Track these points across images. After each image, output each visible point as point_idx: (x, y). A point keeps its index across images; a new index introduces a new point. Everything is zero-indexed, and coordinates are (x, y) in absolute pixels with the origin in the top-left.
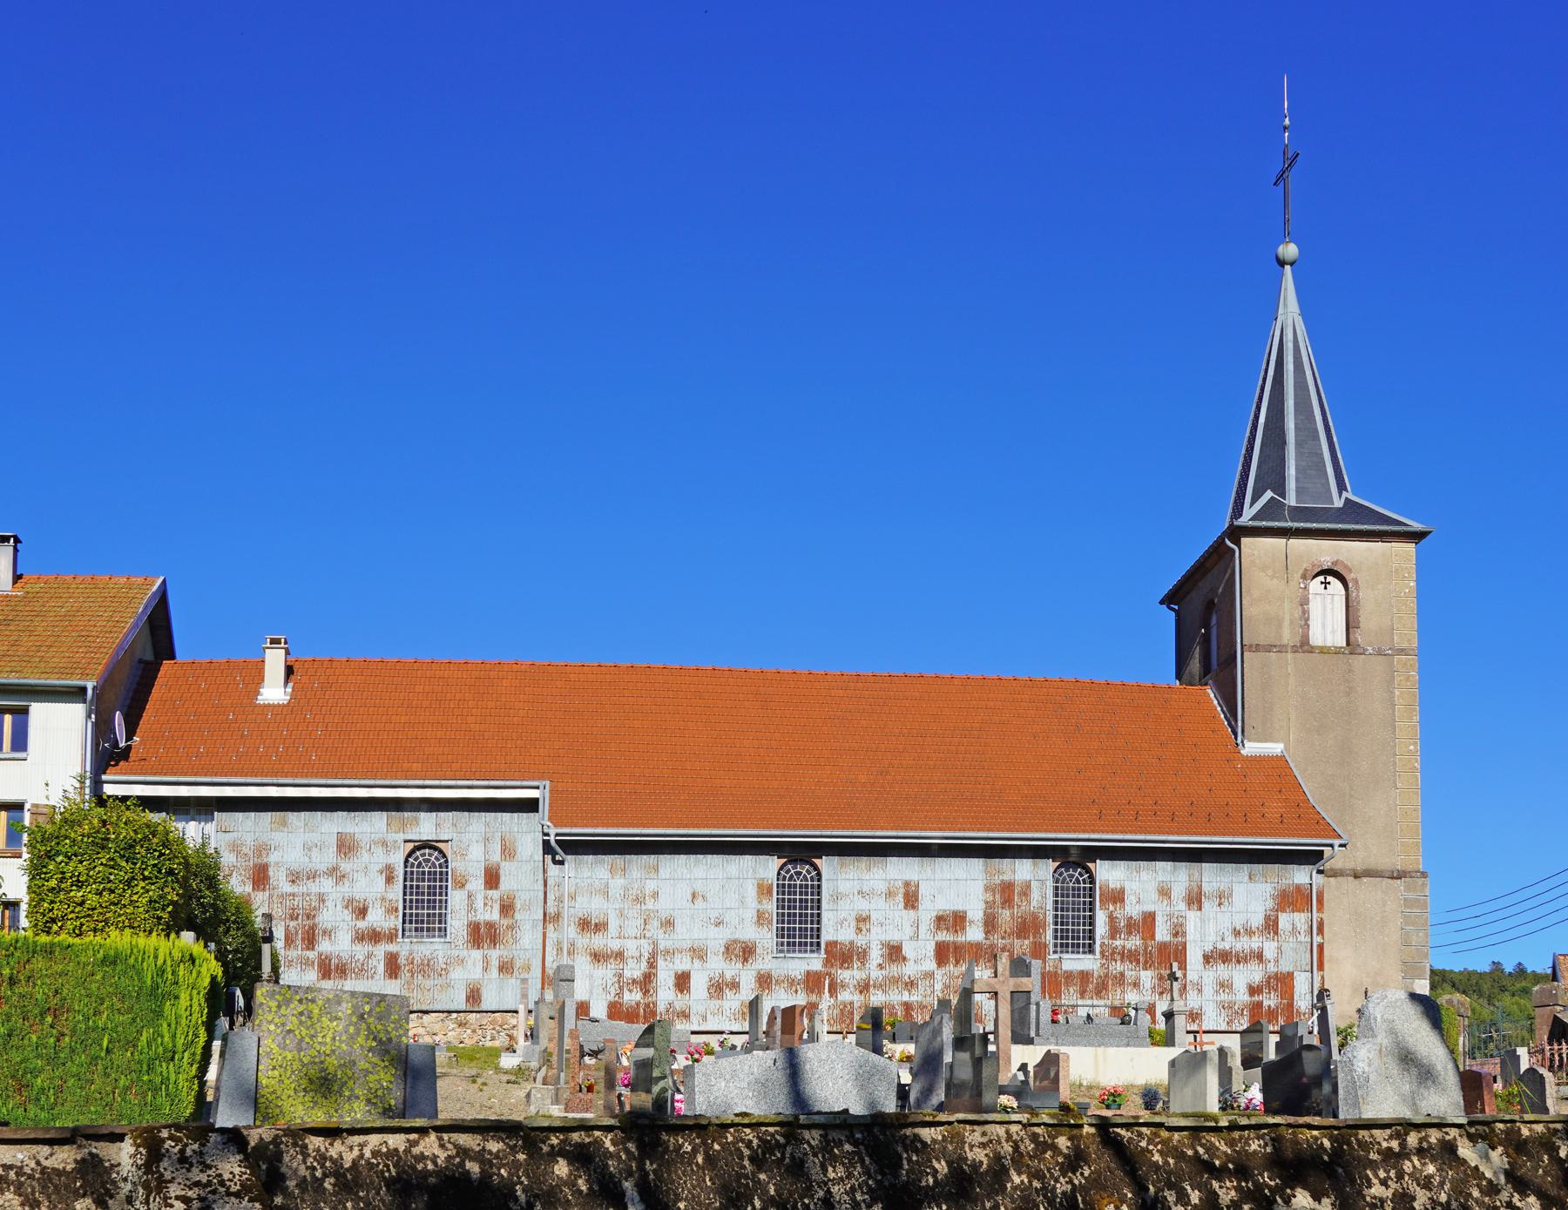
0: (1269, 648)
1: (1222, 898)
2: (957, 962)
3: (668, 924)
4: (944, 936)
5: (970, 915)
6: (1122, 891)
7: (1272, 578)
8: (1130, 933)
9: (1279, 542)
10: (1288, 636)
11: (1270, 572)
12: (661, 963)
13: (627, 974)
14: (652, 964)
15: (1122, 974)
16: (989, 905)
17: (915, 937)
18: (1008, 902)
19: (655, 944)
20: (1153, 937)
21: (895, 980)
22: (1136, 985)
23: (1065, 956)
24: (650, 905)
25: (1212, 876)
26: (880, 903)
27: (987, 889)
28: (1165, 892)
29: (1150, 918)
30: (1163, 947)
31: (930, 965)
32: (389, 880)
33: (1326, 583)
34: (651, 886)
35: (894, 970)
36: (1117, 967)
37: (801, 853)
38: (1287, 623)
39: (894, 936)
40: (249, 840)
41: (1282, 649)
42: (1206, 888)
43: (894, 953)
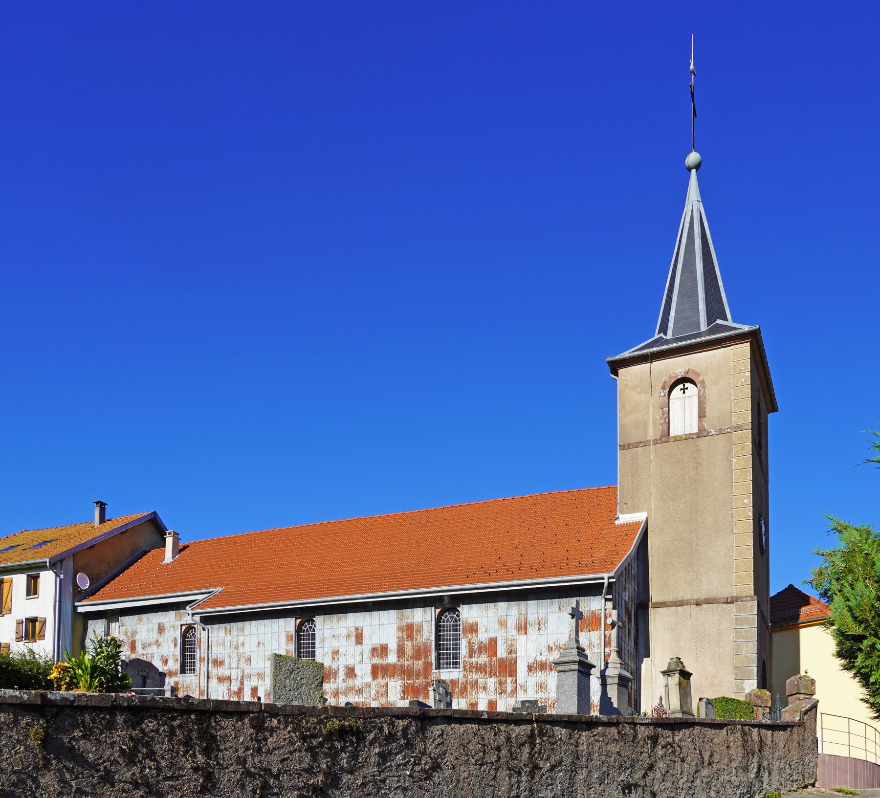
0: (636, 445)
1: (541, 625)
2: (383, 676)
3: (249, 660)
4: (376, 661)
5: (390, 647)
6: (476, 624)
7: (640, 393)
8: (480, 653)
9: (644, 367)
10: (652, 433)
11: (639, 390)
12: (246, 682)
13: (232, 689)
14: (242, 683)
15: (476, 681)
16: (400, 639)
17: (362, 662)
18: (410, 637)
19: (243, 671)
20: (495, 654)
21: (352, 689)
22: (485, 688)
23: (441, 670)
24: (241, 650)
25: (534, 609)
26: (343, 641)
27: (400, 629)
28: (503, 624)
29: (493, 642)
30: (502, 662)
31: (369, 679)
32: (175, 645)
33: (684, 390)
34: (241, 639)
35: (350, 683)
36: (473, 676)
37: (306, 615)
38: (651, 424)
39: (351, 662)
40: (130, 629)
41: (645, 444)
42: (530, 618)
43: (351, 672)
